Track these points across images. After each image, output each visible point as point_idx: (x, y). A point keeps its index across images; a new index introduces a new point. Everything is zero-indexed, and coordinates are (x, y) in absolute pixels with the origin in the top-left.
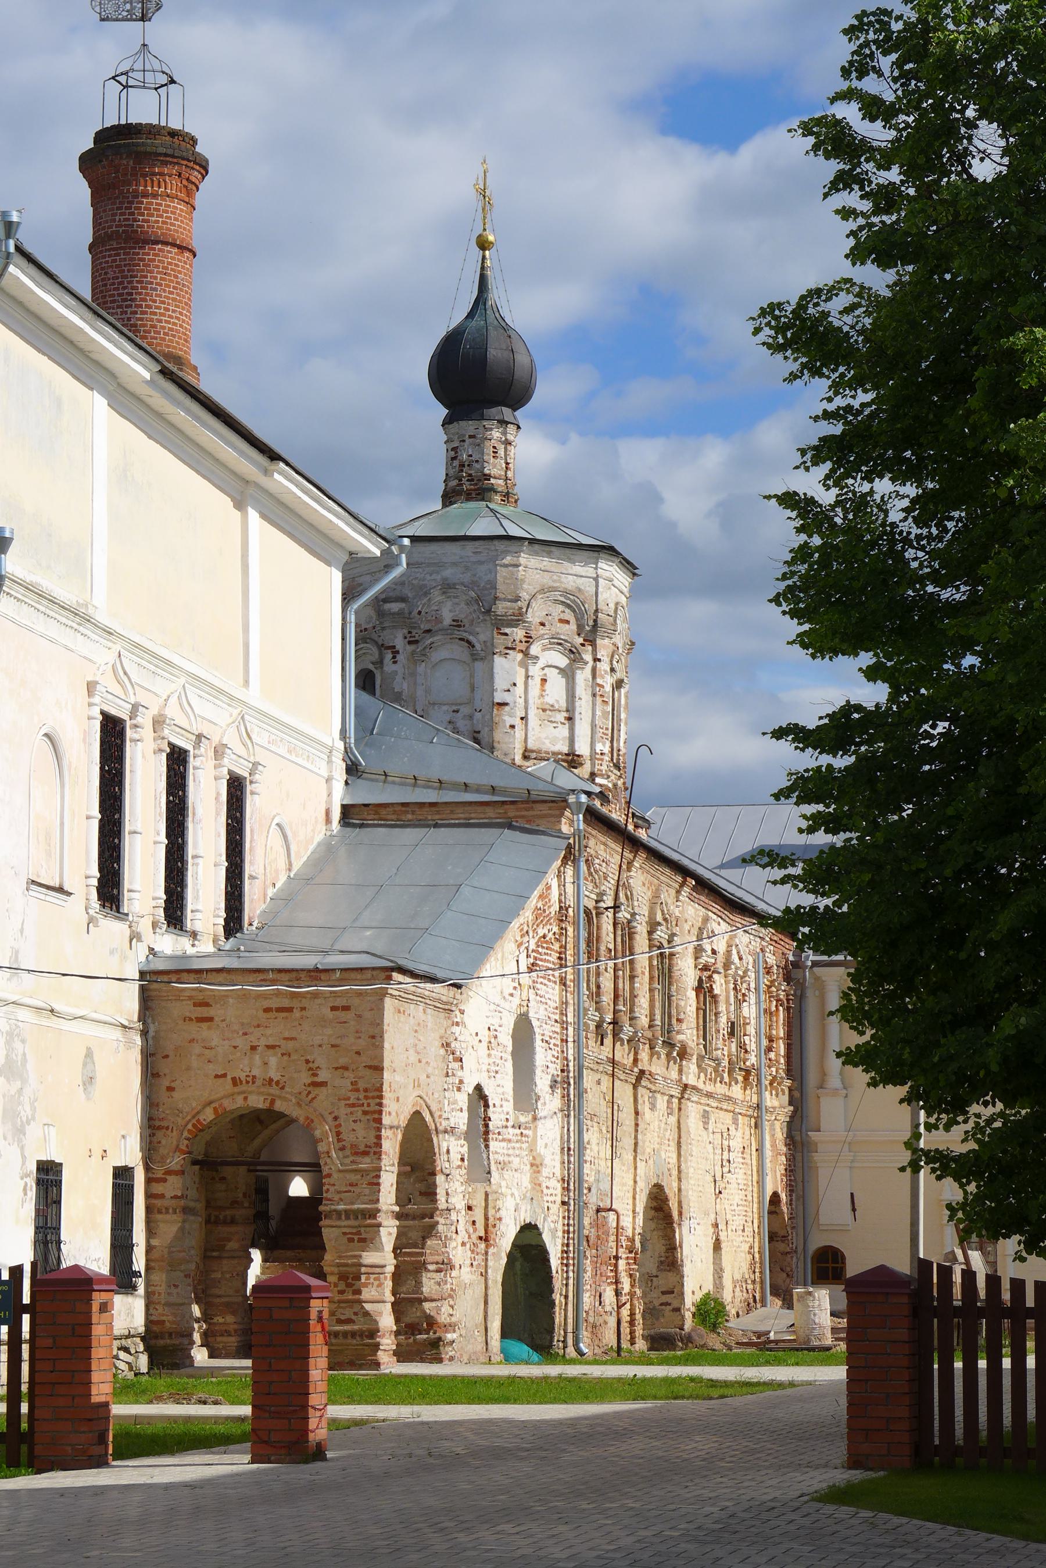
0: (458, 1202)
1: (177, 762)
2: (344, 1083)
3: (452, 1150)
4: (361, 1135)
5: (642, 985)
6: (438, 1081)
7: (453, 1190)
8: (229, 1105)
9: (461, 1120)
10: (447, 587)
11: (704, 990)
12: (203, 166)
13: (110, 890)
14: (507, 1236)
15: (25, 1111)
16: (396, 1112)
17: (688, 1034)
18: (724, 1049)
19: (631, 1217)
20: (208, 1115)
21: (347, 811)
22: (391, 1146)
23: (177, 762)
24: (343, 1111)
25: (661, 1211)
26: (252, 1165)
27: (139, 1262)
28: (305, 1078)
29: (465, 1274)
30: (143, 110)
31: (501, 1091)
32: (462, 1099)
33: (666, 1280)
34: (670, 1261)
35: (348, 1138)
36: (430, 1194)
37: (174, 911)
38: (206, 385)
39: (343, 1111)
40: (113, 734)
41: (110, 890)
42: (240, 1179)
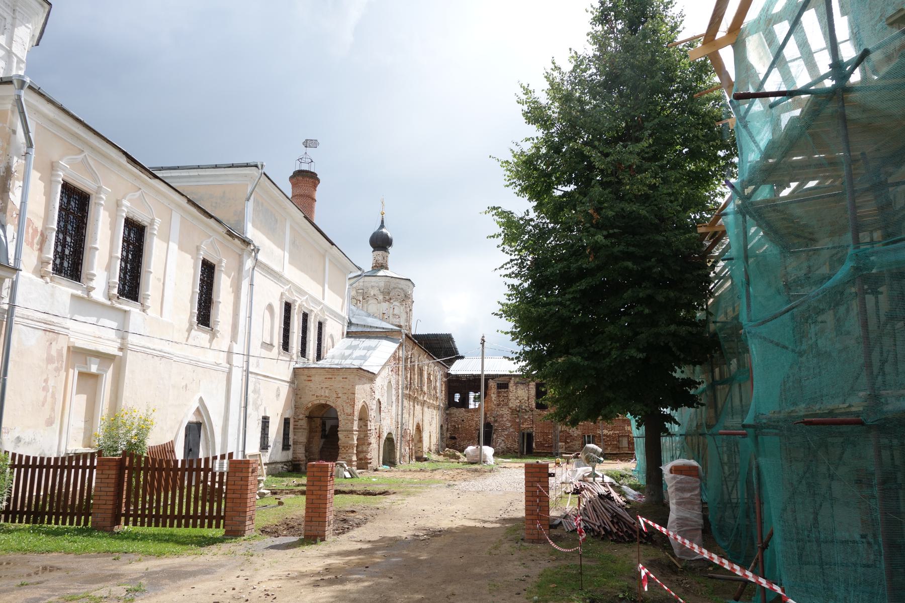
0: (373, 428)
1: (305, 317)
2: (345, 397)
3: (372, 414)
4: (349, 411)
5: (416, 376)
6: (369, 397)
7: (372, 425)
8: (316, 402)
9: (374, 407)
10: (372, 287)
11: (429, 379)
12: (319, 181)
13: (286, 346)
14: (385, 435)
15: (259, 402)
16: (358, 406)
17: (425, 389)
18: (433, 392)
19: (412, 429)
20: (310, 405)
21: (348, 333)
22: (356, 413)
23: (305, 317)
24: (344, 404)
25: (419, 429)
26: (321, 418)
27: (291, 443)
28: (335, 396)
29: (374, 445)
30: (305, 167)
31: (384, 401)
32: (375, 402)
33: (419, 445)
34: (420, 440)
35: (346, 411)
36: (366, 425)
37: (303, 352)
38: (315, 221)
39: (344, 404)
40: (288, 307)
41: (286, 346)
42: (318, 422)
